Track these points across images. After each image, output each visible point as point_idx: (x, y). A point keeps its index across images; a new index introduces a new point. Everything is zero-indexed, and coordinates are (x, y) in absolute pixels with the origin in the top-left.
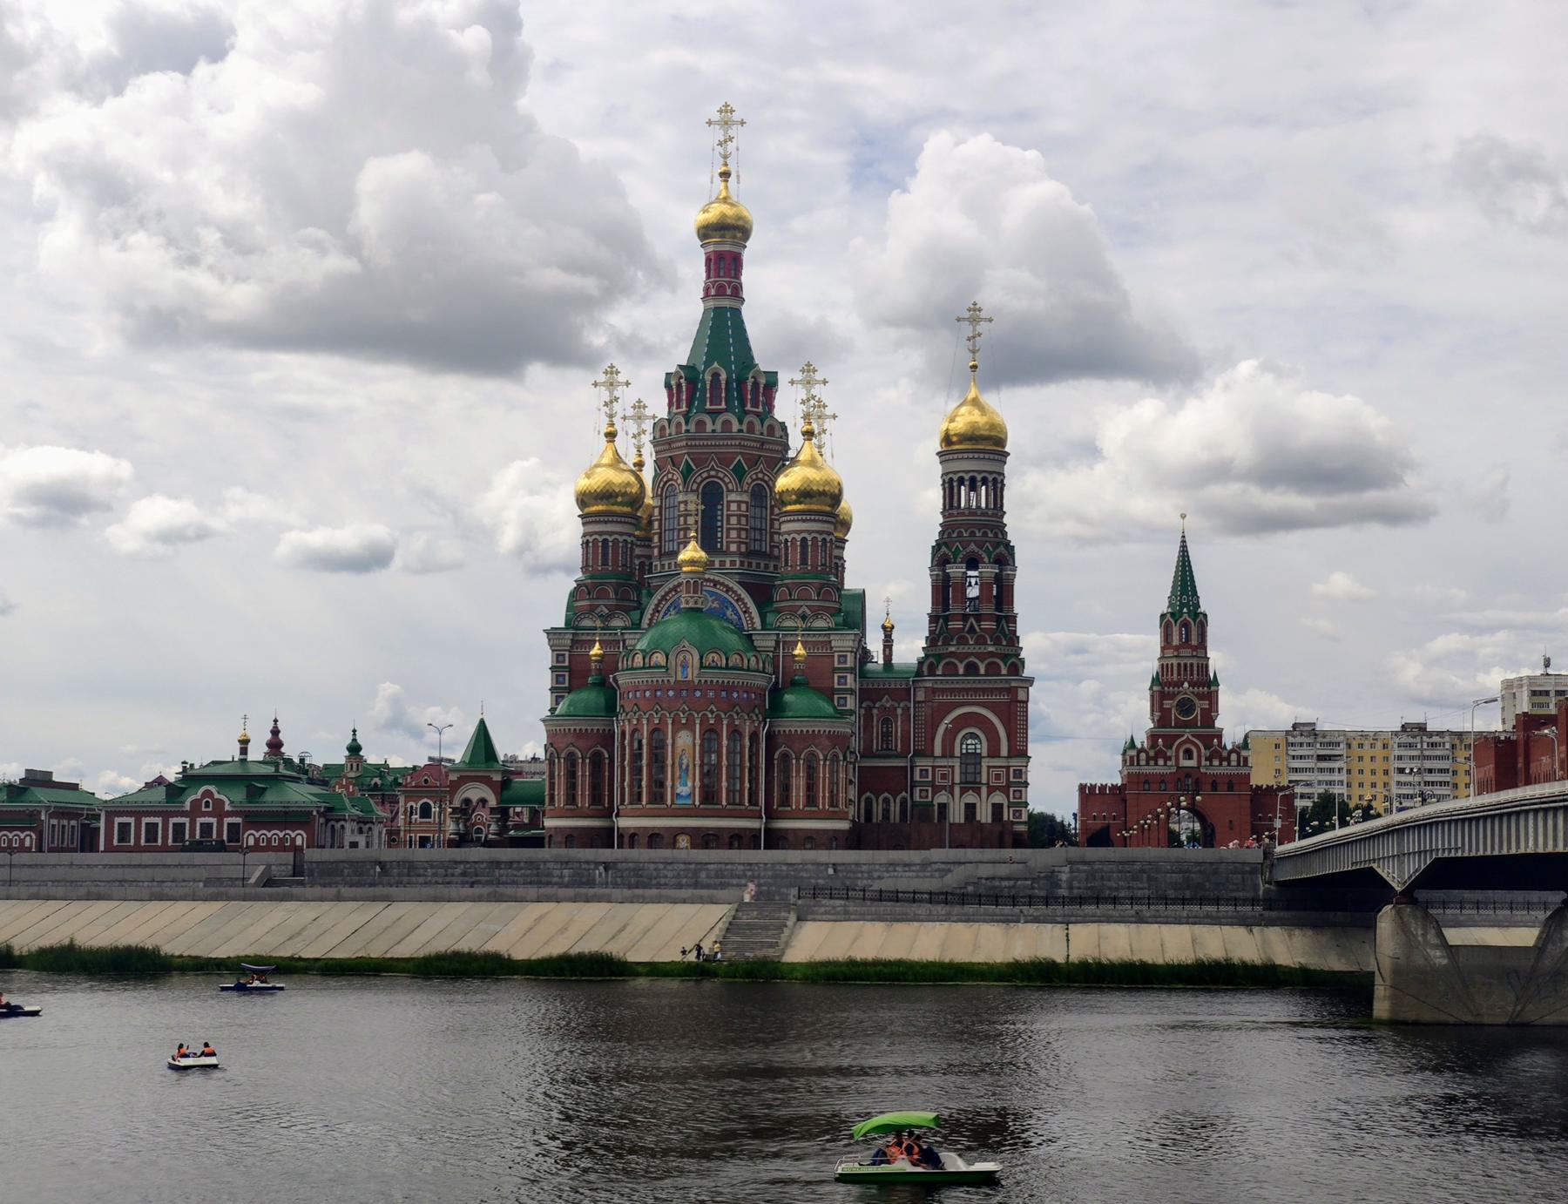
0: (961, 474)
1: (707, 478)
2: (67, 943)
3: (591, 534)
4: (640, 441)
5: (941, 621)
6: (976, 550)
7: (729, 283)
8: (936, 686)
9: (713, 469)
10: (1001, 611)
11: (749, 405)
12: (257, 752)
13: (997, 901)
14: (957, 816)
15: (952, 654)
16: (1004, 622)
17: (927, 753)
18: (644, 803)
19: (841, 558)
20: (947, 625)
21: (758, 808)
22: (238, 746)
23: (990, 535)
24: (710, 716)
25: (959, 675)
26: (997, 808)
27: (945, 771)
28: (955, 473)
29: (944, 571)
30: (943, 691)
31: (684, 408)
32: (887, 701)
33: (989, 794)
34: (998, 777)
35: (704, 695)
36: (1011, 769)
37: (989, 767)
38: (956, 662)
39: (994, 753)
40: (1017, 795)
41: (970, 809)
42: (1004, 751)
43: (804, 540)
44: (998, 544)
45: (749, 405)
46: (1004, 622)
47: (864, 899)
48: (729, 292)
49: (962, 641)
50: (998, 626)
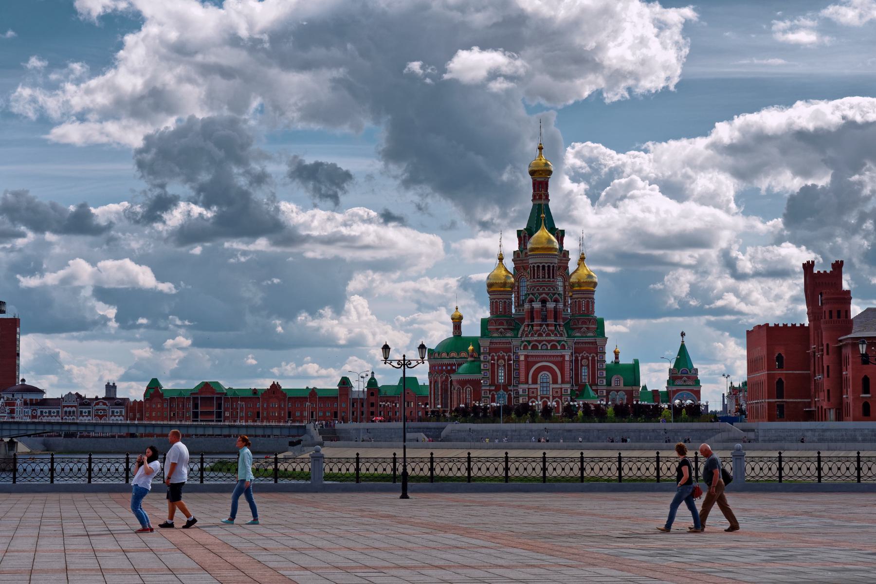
2: (109, 317)
3: (553, 281)
6: (546, 296)
8: (529, 354)
15: (536, 341)
19: (593, 299)
20: (533, 329)
27: (554, 393)
28: (535, 263)
29: (531, 305)
30: (532, 356)
34: (557, 392)
37: (553, 388)
38: (538, 344)
39: (555, 381)
42: (560, 380)
44: (555, 293)
46: (558, 327)
49: (540, 335)
50: (555, 328)
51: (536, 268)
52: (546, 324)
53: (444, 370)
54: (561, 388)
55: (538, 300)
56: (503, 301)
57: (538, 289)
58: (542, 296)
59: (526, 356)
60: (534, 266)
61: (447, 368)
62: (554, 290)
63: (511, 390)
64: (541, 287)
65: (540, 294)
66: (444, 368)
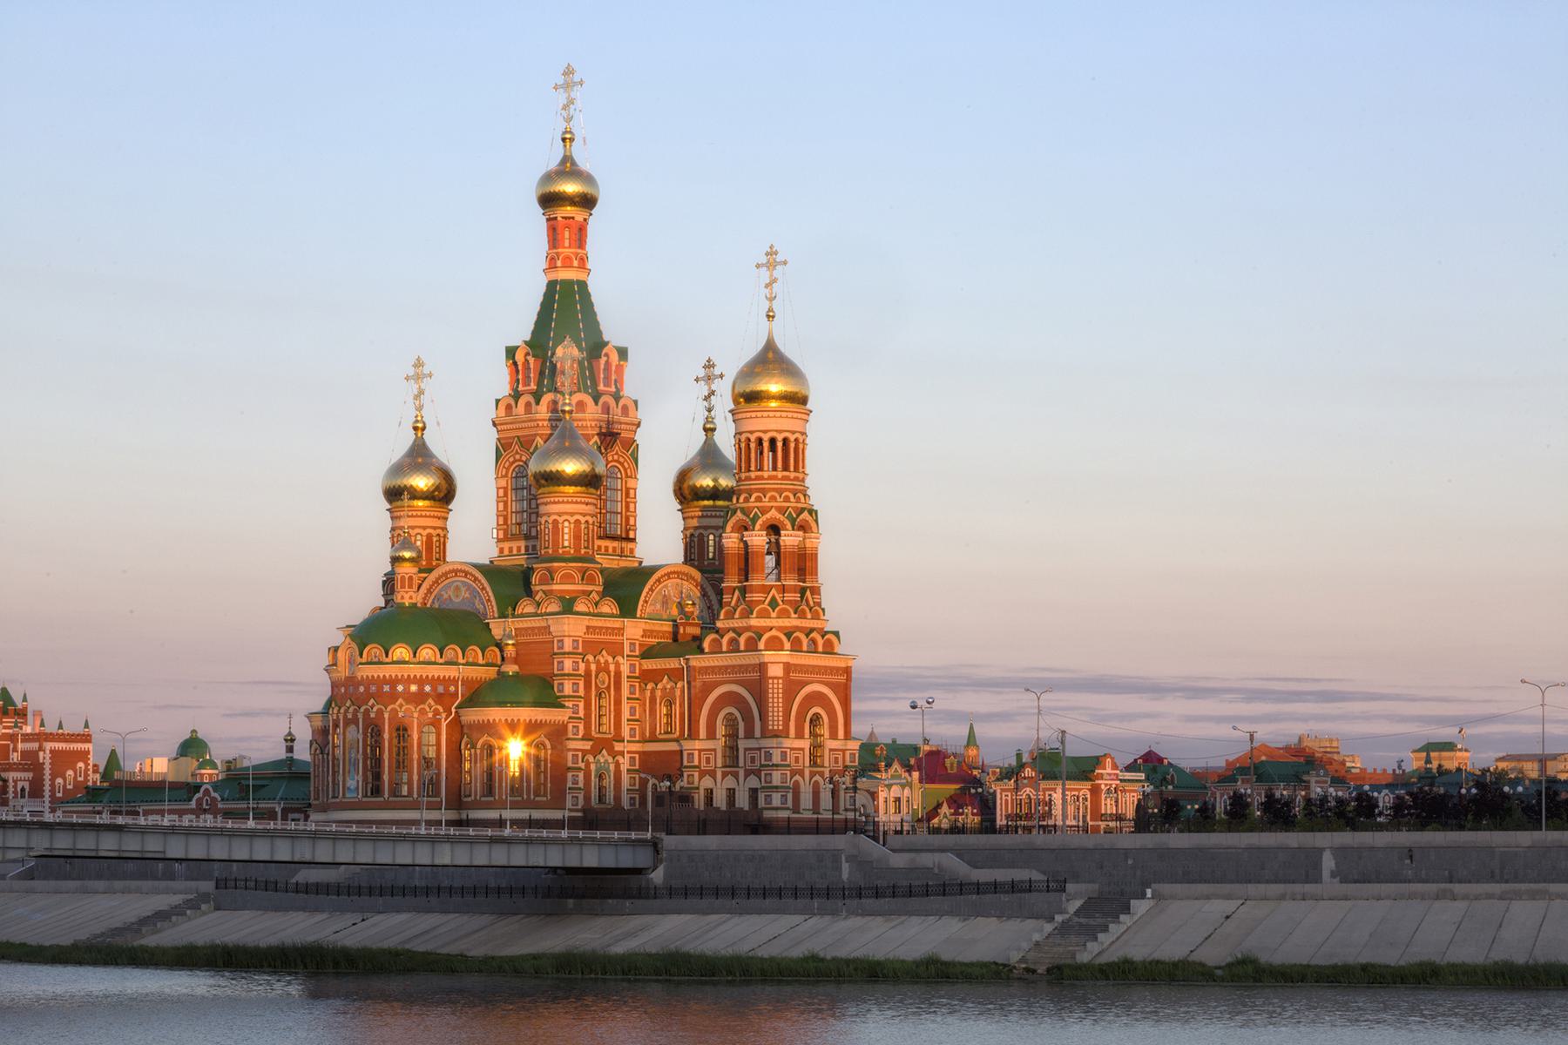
0: (787, 434)
1: (513, 462)
4: (710, 404)
5: (737, 593)
6: (779, 516)
7: (576, 254)
9: (517, 453)
10: (804, 582)
11: (602, 385)
12: (303, 753)
13: (961, 890)
14: (741, 803)
16: (808, 593)
17: (693, 735)
18: (386, 796)
21: (439, 799)
22: (284, 744)
23: (792, 499)
24: (428, 710)
25: (722, 652)
26: (754, 793)
31: (533, 387)
32: (668, 683)
33: (746, 777)
35: (367, 689)
36: (848, 752)
37: (746, 749)
40: (768, 778)
41: (731, 794)
42: (841, 733)
43: (429, 537)
44: (802, 510)
45: (602, 385)
47: (236, 880)
48: (576, 263)
50: (802, 597)
51: (753, 446)
52: (544, 592)
53: (428, 695)
54: (844, 751)
55: (757, 526)
56: (572, 519)
57: (759, 499)
58: (768, 516)
59: (788, 667)
60: (760, 441)
61: (434, 689)
62: (798, 501)
63: (622, 753)
64: (780, 492)
65: (764, 511)
66: (400, 688)
